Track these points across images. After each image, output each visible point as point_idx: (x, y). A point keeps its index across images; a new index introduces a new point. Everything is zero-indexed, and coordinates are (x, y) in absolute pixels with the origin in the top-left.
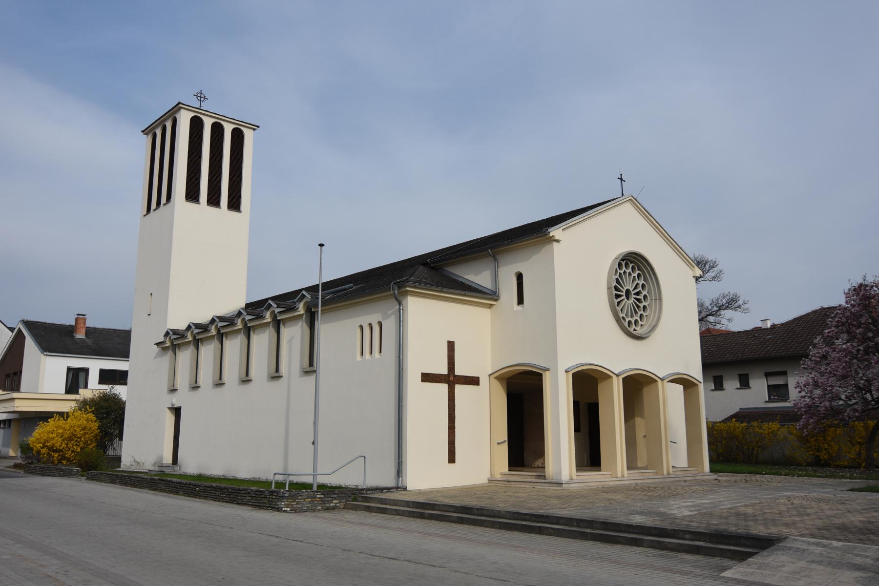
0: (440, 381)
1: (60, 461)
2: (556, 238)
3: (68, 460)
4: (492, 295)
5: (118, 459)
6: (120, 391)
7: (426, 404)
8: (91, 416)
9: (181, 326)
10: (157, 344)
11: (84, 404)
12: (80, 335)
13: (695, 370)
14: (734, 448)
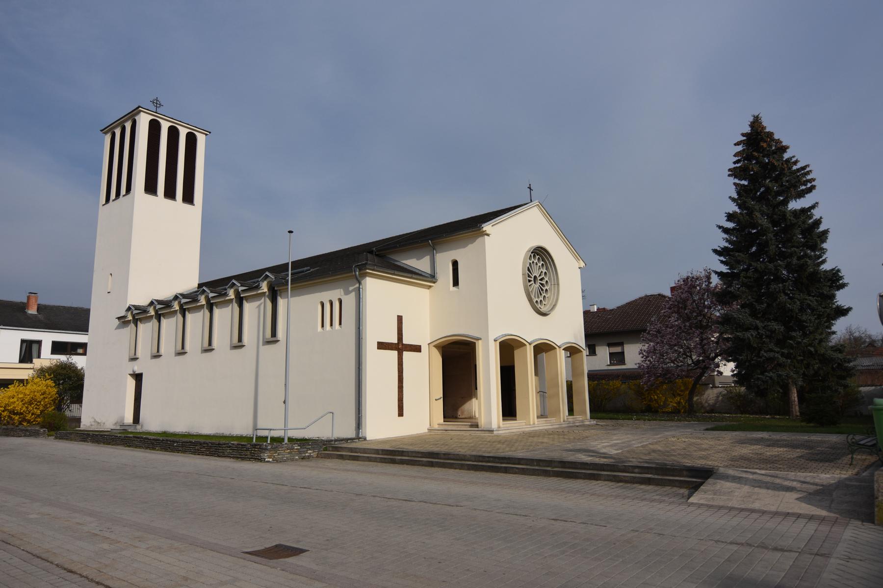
0: (392, 349)
1: (20, 423)
2: (488, 232)
3: (29, 421)
4: (432, 278)
5: (78, 420)
6: (79, 361)
7: (380, 366)
8: (50, 382)
9: (143, 302)
10: (119, 318)
11: (42, 372)
12: (32, 311)
13: (581, 342)
14: (611, 398)
